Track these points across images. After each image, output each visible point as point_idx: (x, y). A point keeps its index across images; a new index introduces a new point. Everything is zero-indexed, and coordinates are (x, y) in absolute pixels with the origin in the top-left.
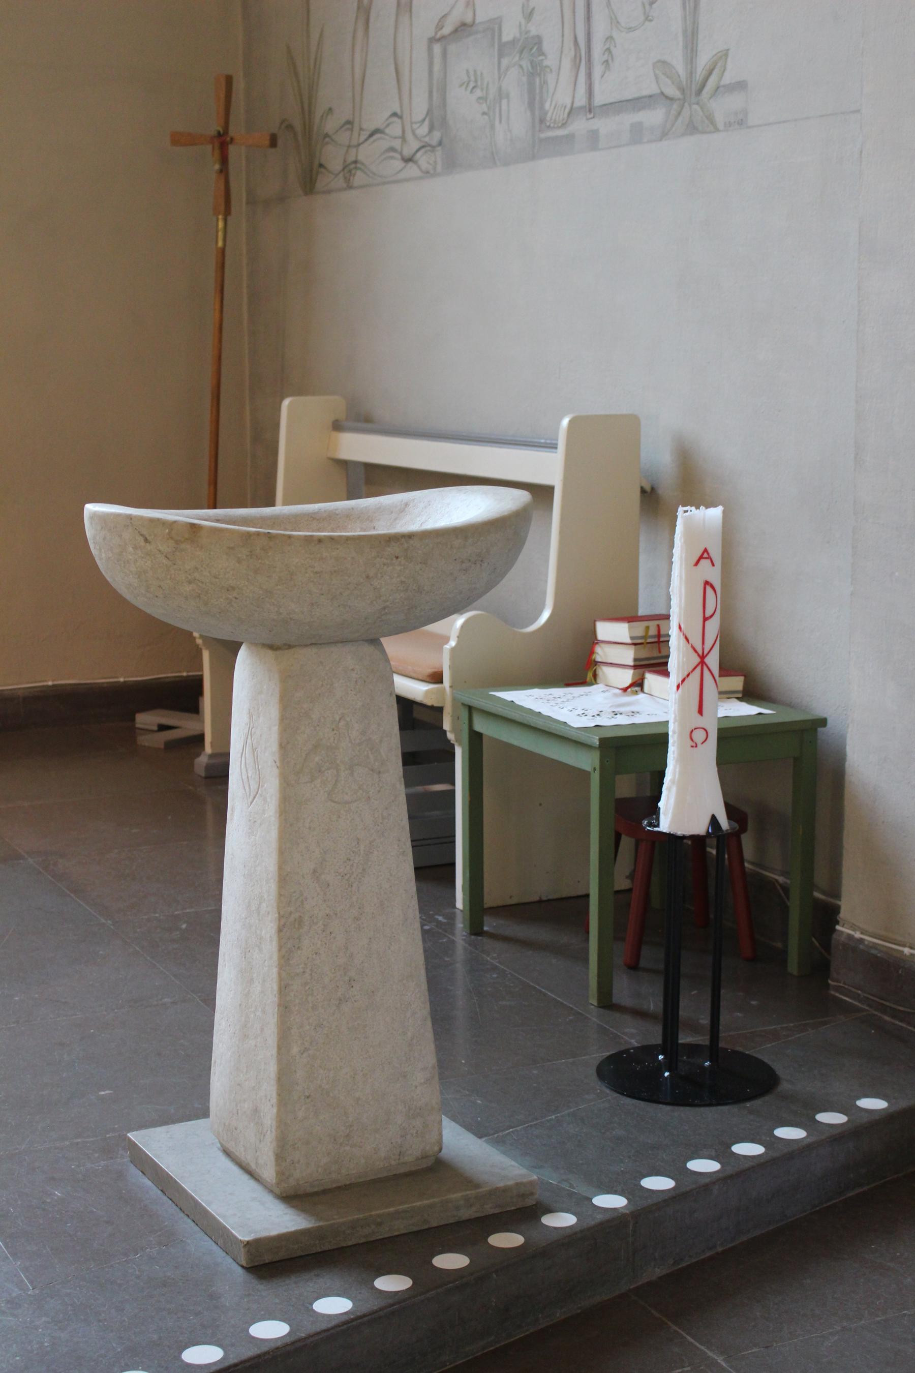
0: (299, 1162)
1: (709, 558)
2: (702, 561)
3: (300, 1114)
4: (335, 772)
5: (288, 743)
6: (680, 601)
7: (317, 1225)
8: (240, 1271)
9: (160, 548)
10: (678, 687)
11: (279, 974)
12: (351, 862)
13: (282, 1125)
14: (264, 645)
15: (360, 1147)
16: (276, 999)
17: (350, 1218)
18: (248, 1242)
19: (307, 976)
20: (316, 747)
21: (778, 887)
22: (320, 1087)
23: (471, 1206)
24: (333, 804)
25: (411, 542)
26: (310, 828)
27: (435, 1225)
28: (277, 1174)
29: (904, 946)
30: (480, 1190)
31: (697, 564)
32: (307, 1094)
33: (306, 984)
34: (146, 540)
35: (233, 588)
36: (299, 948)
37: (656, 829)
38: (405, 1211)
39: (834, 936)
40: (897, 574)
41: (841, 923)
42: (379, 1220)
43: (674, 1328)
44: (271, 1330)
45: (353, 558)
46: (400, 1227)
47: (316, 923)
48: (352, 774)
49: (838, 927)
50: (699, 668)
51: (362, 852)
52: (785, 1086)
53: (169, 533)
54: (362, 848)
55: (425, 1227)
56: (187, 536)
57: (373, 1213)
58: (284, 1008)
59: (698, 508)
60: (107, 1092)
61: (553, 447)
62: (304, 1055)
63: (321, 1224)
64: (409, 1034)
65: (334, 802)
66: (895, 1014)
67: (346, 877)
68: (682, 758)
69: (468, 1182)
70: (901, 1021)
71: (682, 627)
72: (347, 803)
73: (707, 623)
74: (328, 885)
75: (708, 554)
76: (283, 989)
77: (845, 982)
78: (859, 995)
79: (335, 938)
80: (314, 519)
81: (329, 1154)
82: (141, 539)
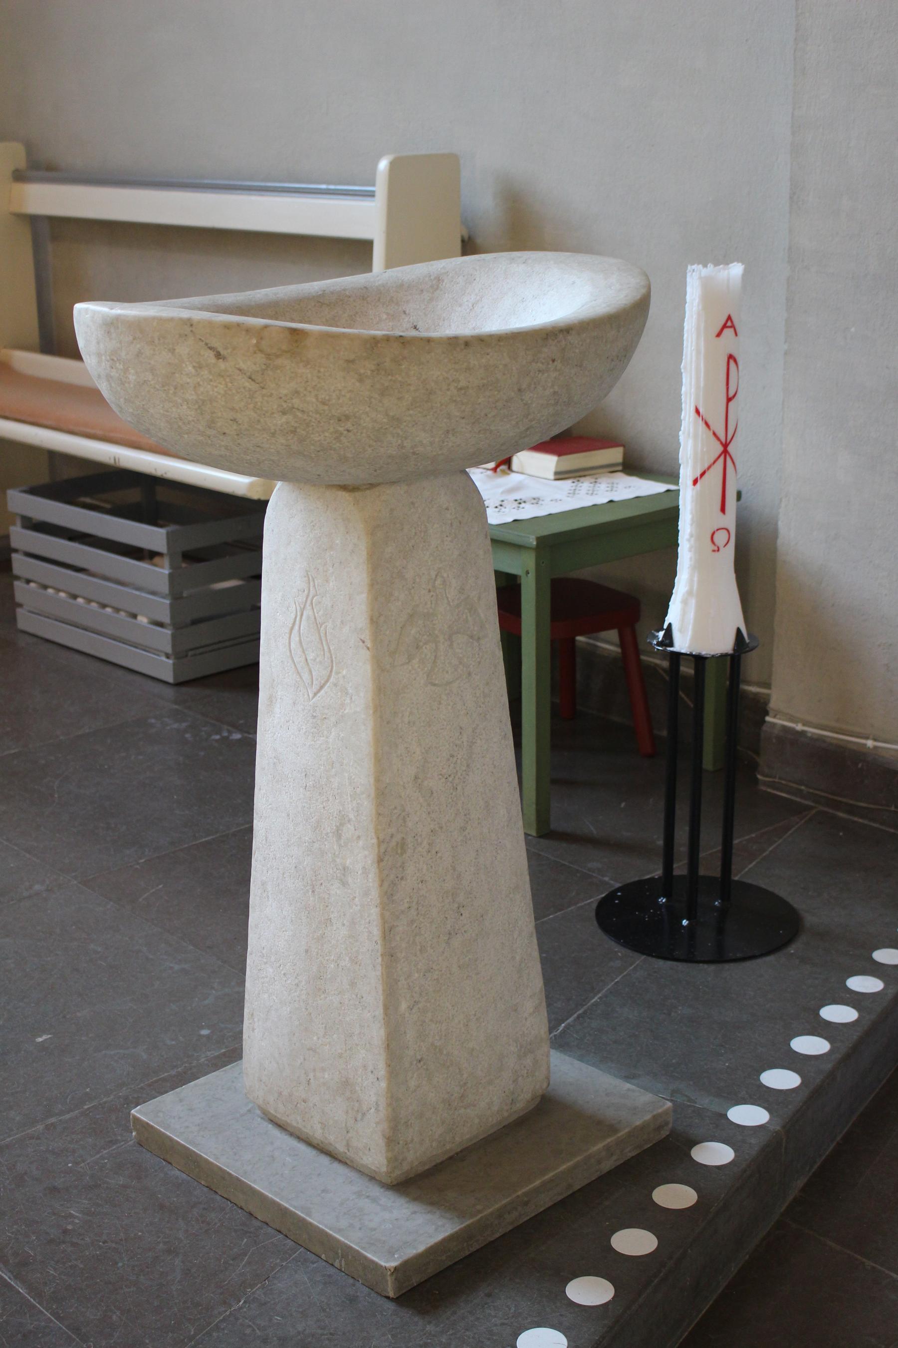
0: (412, 1140)
1: (733, 326)
2: (726, 331)
3: (413, 1083)
5: (380, 615)
6: (698, 379)
7: (463, 1226)
8: (391, 1306)
9: (242, 366)
10: (695, 482)
11: (382, 916)
13: (394, 1100)
14: (330, 486)
15: (475, 1106)
16: (379, 947)
17: (497, 1206)
18: (396, 1268)
19: (413, 912)
21: (661, 671)
22: (432, 1044)
23: (612, 1155)
25: (569, 338)
28: (389, 1161)
29: (867, 738)
30: (619, 1135)
31: (719, 335)
32: (419, 1057)
33: (412, 922)
34: (218, 356)
35: (347, 418)
36: (402, 878)
37: (671, 649)
38: (551, 1180)
39: (764, 728)
40: (853, 330)
41: (771, 713)
42: (526, 1199)
43: (869, 1263)
45: (505, 365)
46: (545, 1201)
48: (451, 646)
49: (768, 719)
50: (722, 458)
52: (809, 920)
53: (257, 345)
54: (465, 739)
55: (570, 1192)
56: (284, 347)
57: (519, 1193)
58: (390, 956)
59: (705, 266)
60: (45, 1037)
61: (371, 195)
62: (414, 1011)
63: (468, 1222)
64: (518, 958)
65: (435, 685)
66: (852, 810)
67: (450, 779)
68: (699, 565)
69: (601, 1126)
70: (861, 817)
71: (701, 411)
72: (449, 683)
73: (731, 404)
75: (732, 322)
76: (388, 932)
77: (774, 776)
78: (801, 791)
79: (441, 858)
80: (323, 304)
81: (443, 1123)
82: (209, 356)
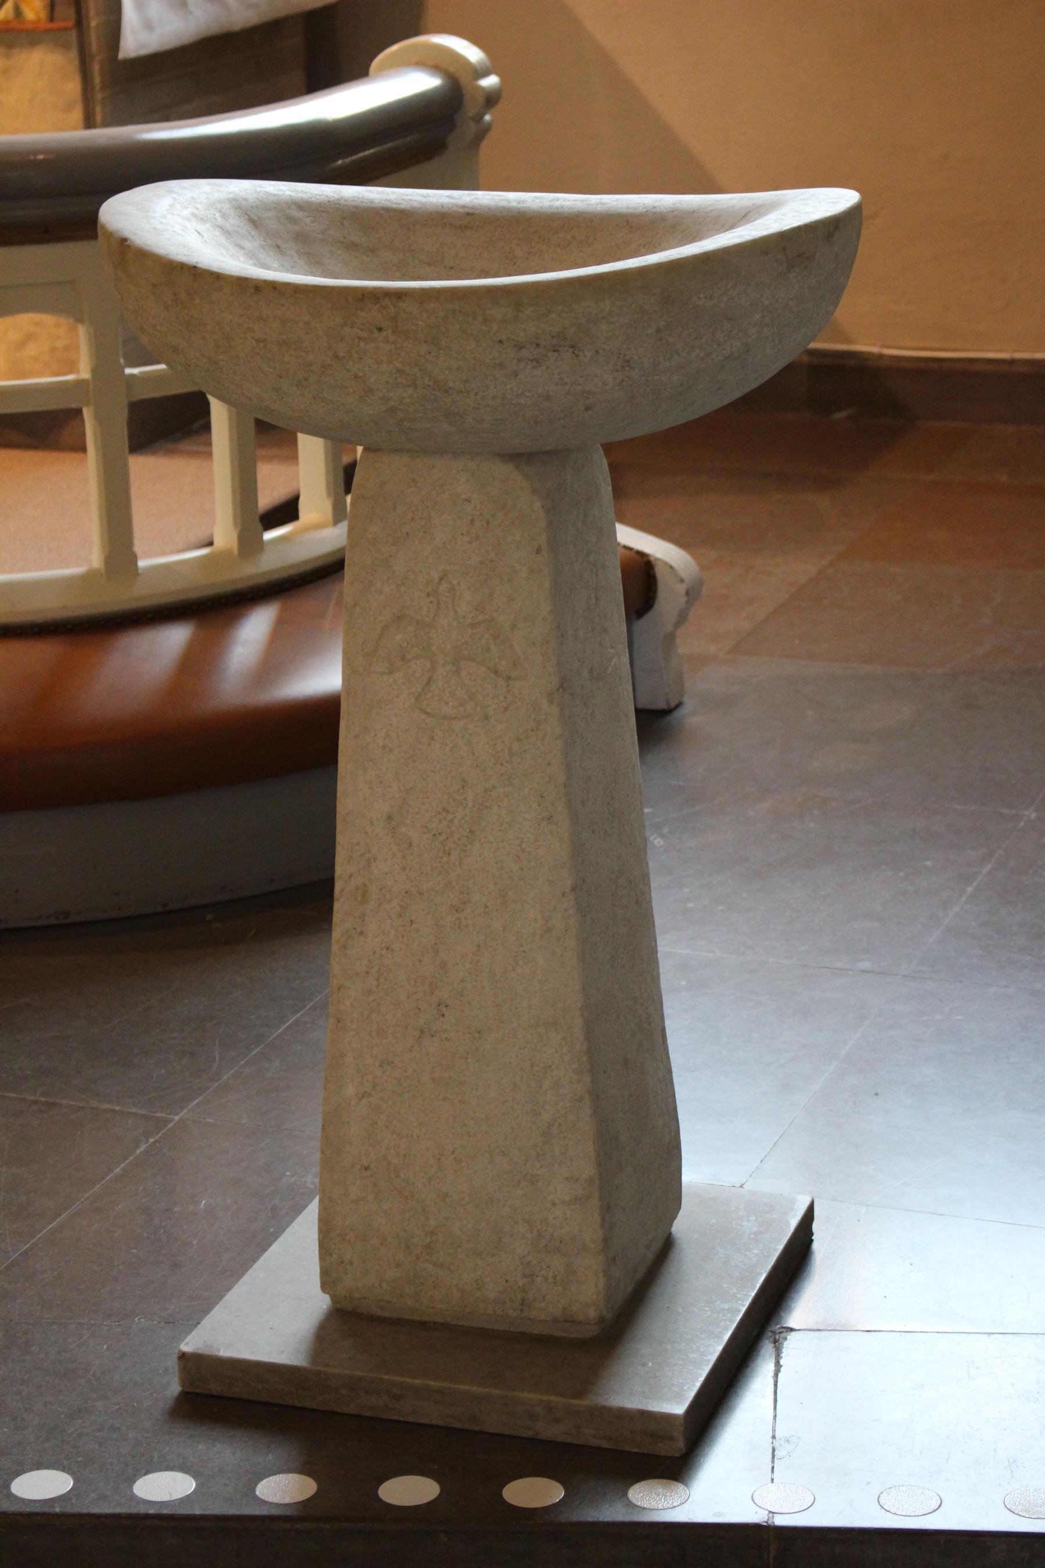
4: (428, 665)
12: (451, 816)
20: (400, 618)
24: (424, 717)
26: (384, 747)
27: (492, 1430)
33: (370, 992)
36: (361, 933)
44: (164, 1488)
45: (307, 323)
46: (433, 1414)
47: (390, 901)
48: (457, 672)
51: (470, 804)
62: (364, 1101)
65: (428, 714)
67: (441, 838)
74: (411, 845)
